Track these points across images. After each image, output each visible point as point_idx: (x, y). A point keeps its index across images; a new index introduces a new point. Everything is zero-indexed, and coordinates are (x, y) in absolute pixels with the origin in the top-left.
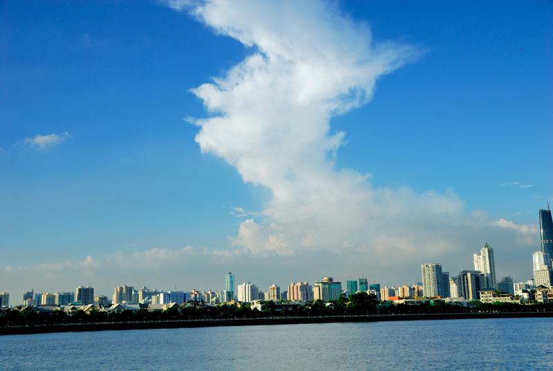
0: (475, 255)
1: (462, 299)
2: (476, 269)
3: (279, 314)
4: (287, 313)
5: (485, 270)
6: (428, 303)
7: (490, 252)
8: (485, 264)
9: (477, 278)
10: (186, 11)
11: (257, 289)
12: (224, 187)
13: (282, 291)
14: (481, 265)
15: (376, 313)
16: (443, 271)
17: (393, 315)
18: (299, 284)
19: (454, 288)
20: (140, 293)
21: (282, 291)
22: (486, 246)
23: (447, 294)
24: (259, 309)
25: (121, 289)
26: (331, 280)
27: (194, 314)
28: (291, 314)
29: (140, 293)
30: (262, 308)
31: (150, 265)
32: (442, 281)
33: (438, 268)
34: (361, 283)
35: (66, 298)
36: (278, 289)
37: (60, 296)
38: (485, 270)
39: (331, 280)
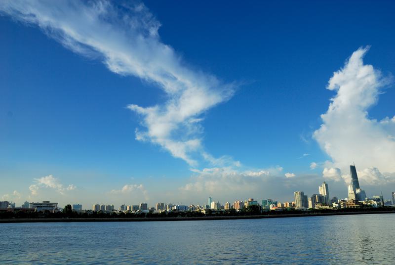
0: (320, 187)
1: (303, 208)
2: (320, 194)
3: (214, 215)
4: (217, 215)
5: (324, 194)
6: (109, 214)
7: (326, 185)
8: (324, 191)
9: (320, 197)
10: (378, 121)
11: (220, 204)
12: (154, 154)
13: (231, 205)
14: (322, 191)
15: (260, 215)
16: (304, 195)
17: (68, 218)
18: (239, 202)
19: (310, 203)
20: (168, 206)
21: (231, 205)
22: (324, 183)
23: (307, 206)
24: (205, 213)
25: (159, 204)
26: (252, 200)
27: (71, 215)
28: (219, 215)
29: (168, 206)
30: (206, 212)
31: (122, 193)
32: (304, 201)
33: (302, 194)
34: (268, 201)
35: (136, 208)
36: (229, 204)
37: (133, 207)
38: (324, 194)
39: (252, 200)
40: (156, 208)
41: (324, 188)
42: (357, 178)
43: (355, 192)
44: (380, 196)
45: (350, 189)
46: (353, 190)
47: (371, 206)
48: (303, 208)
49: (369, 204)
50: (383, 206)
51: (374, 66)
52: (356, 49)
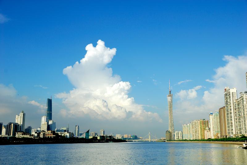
0: (17, 116)
1: (7, 136)
2: (16, 122)
5: (20, 123)
7: (24, 115)
8: (21, 120)
9: (16, 126)
14: (19, 120)
38: (20, 123)
40: (46, 131)
41: (21, 117)
42: (51, 111)
43: (48, 123)
44: (67, 128)
45: (44, 119)
46: (46, 121)
47: (64, 136)
48: (7, 136)
49: (63, 135)
50: (73, 136)
51: (101, 40)
52: (199, 85)
